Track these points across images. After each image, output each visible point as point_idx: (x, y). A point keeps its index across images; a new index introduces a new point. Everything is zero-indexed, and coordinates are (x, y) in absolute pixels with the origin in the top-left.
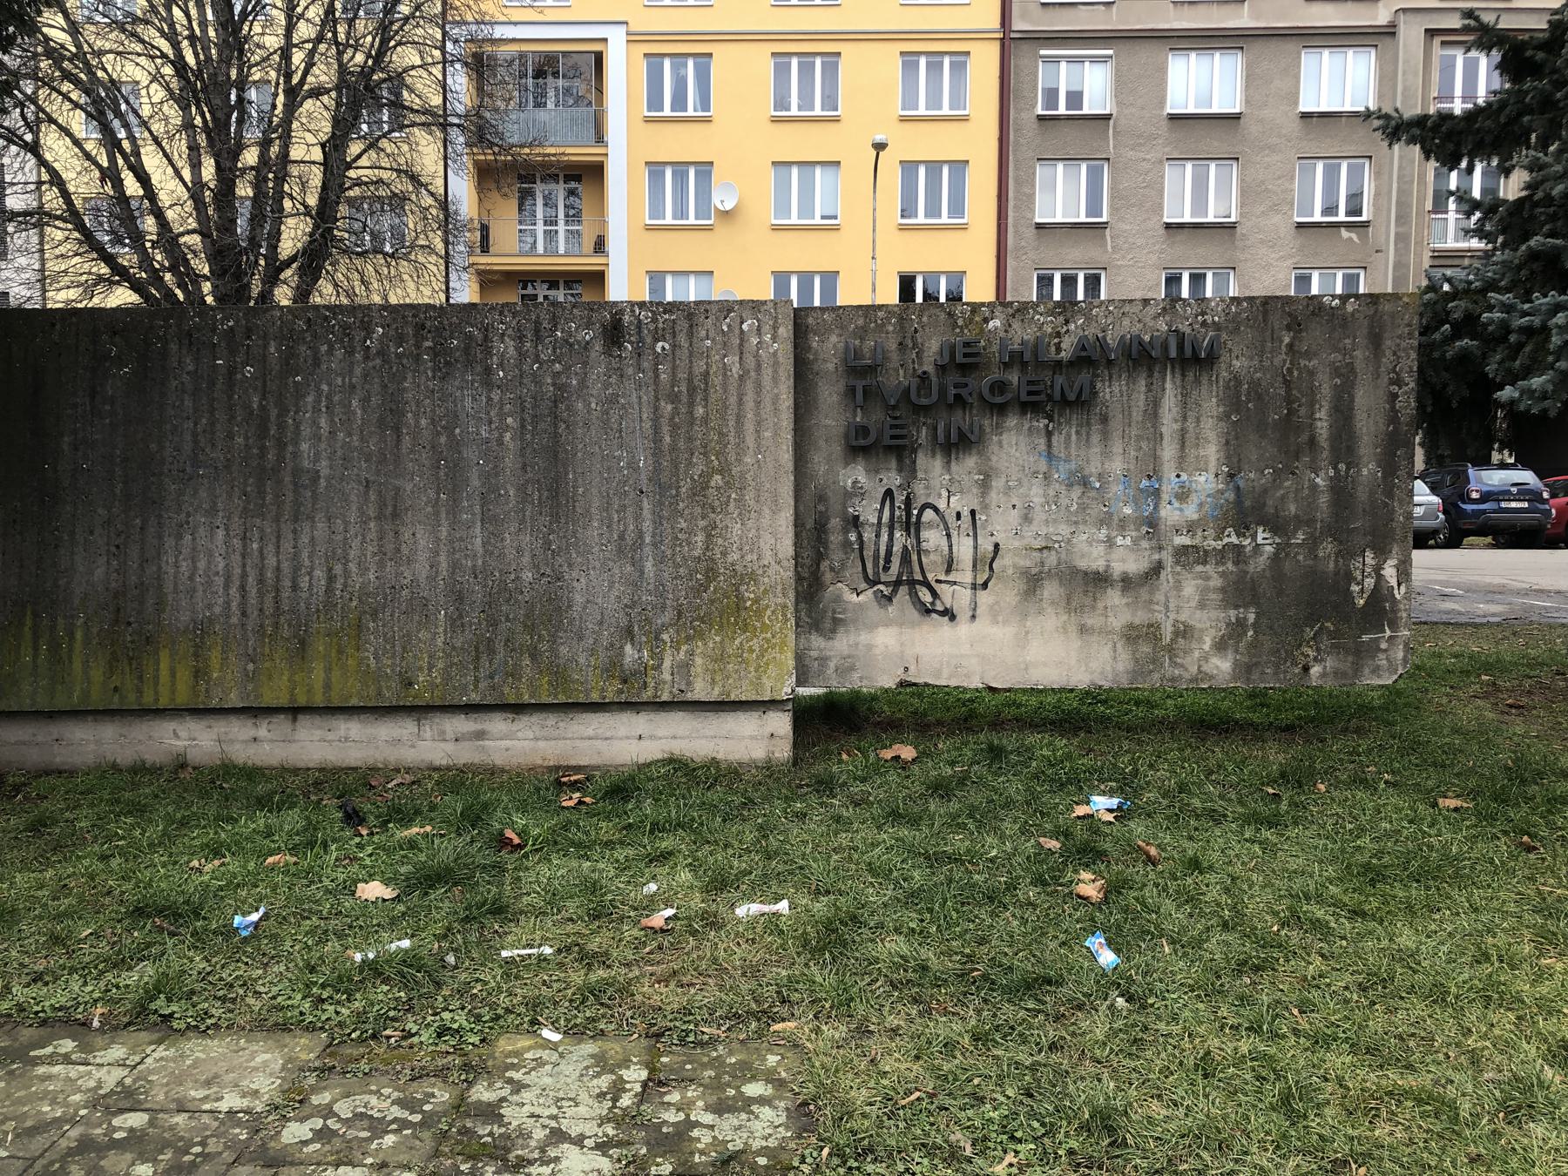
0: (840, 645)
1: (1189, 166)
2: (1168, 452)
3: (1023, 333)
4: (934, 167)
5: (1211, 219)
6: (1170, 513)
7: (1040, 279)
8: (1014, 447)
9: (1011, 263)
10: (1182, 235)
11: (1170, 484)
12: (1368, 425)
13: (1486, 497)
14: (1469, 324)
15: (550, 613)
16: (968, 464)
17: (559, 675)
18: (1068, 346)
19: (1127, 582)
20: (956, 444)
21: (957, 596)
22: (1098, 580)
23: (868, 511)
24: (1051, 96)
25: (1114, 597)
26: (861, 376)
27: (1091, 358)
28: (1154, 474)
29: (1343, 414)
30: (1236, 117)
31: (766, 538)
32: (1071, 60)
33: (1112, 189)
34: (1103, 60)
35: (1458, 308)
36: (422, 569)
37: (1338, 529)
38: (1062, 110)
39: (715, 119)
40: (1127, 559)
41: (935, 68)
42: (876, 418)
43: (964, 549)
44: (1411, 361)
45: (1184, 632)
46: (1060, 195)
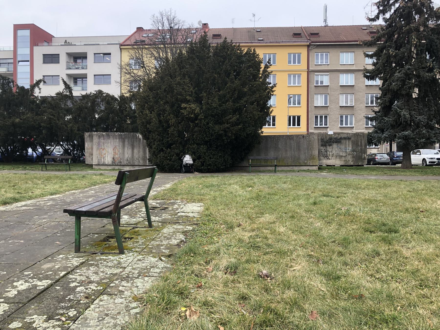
0: (321, 162)
1: (344, 95)
2: (347, 146)
3: (335, 137)
4: (294, 96)
5: (349, 105)
6: (347, 151)
7: (316, 117)
8: (335, 145)
9: (310, 114)
10: (343, 108)
11: (347, 148)
12: (363, 144)
13: (397, 157)
14: (371, 136)
15: (299, 158)
16: (331, 147)
17: (300, 163)
18: (339, 138)
19: (344, 156)
20: (330, 145)
21: (330, 158)
22: (342, 156)
23: (323, 151)
24: (317, 82)
25: (343, 158)
26: (322, 140)
27: (341, 138)
28: (346, 148)
29: (361, 143)
30: (353, 86)
31: (316, 152)
32: (321, 75)
33: (329, 99)
34: (327, 75)
35: (370, 134)
36: (289, 155)
37: (361, 152)
38: (319, 85)
39: (299, 115)
40: (344, 155)
41: (294, 77)
42: (324, 143)
43: (331, 154)
44: (367, 139)
45: (349, 160)
46: (319, 101)
